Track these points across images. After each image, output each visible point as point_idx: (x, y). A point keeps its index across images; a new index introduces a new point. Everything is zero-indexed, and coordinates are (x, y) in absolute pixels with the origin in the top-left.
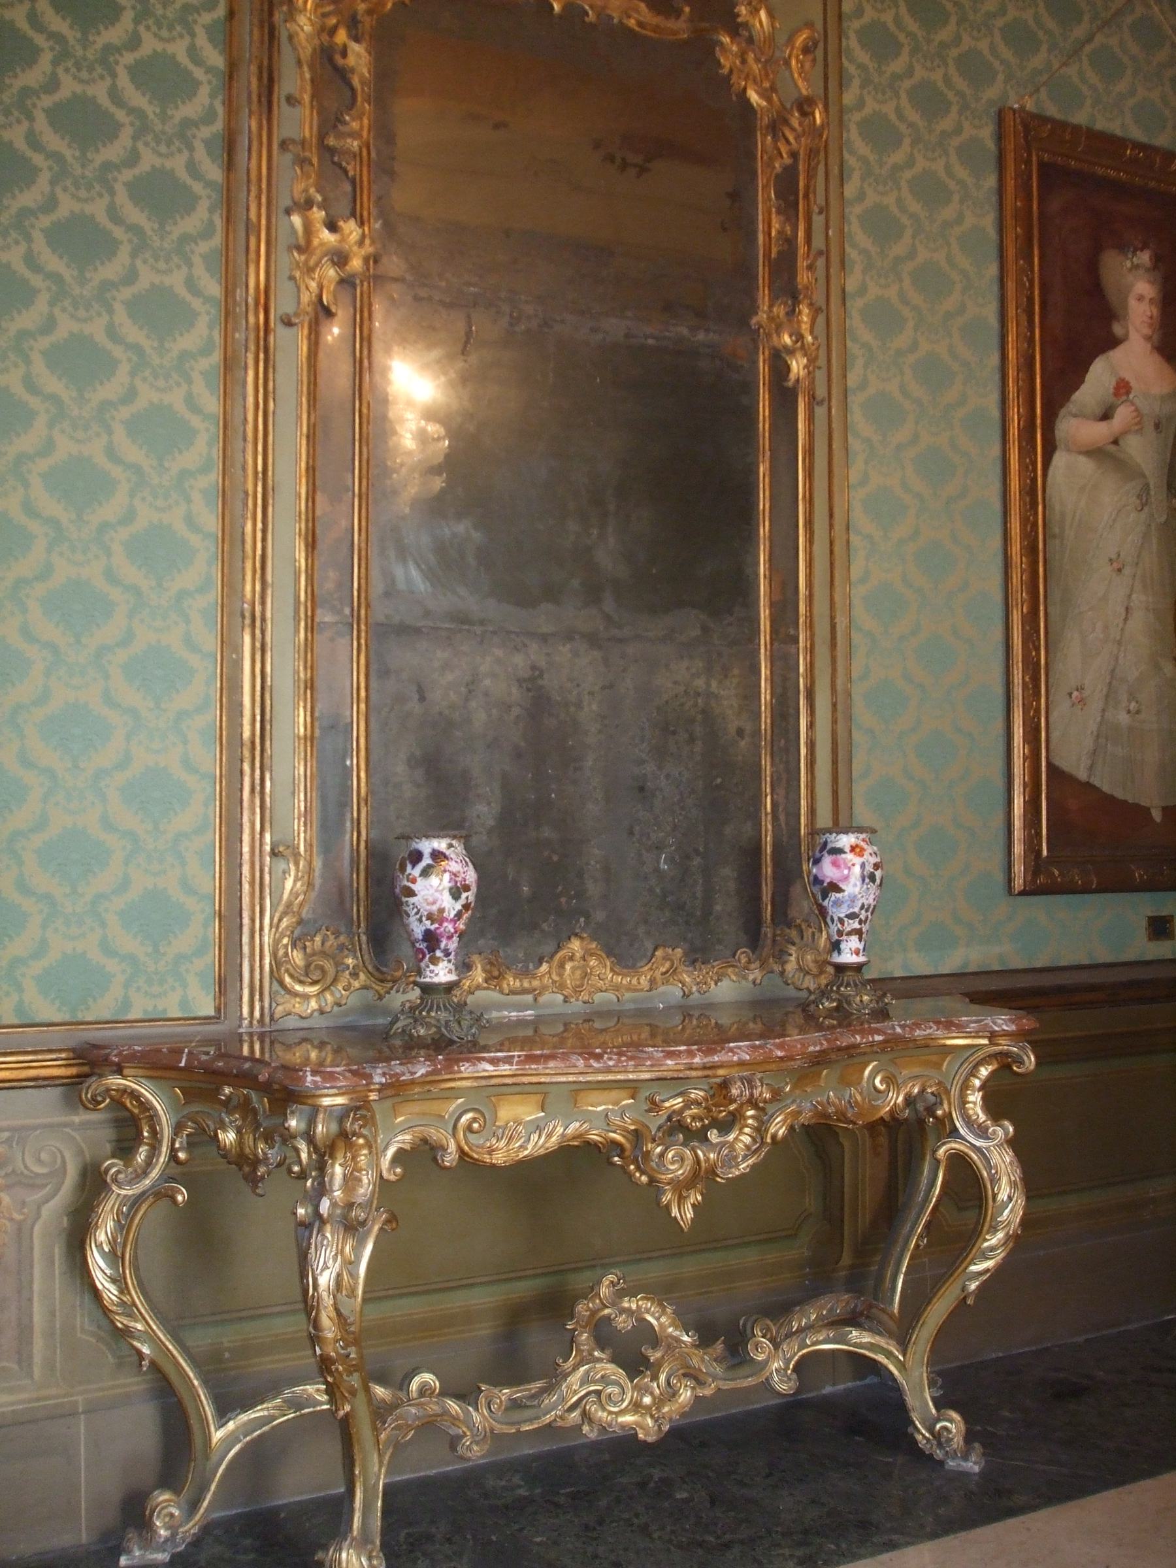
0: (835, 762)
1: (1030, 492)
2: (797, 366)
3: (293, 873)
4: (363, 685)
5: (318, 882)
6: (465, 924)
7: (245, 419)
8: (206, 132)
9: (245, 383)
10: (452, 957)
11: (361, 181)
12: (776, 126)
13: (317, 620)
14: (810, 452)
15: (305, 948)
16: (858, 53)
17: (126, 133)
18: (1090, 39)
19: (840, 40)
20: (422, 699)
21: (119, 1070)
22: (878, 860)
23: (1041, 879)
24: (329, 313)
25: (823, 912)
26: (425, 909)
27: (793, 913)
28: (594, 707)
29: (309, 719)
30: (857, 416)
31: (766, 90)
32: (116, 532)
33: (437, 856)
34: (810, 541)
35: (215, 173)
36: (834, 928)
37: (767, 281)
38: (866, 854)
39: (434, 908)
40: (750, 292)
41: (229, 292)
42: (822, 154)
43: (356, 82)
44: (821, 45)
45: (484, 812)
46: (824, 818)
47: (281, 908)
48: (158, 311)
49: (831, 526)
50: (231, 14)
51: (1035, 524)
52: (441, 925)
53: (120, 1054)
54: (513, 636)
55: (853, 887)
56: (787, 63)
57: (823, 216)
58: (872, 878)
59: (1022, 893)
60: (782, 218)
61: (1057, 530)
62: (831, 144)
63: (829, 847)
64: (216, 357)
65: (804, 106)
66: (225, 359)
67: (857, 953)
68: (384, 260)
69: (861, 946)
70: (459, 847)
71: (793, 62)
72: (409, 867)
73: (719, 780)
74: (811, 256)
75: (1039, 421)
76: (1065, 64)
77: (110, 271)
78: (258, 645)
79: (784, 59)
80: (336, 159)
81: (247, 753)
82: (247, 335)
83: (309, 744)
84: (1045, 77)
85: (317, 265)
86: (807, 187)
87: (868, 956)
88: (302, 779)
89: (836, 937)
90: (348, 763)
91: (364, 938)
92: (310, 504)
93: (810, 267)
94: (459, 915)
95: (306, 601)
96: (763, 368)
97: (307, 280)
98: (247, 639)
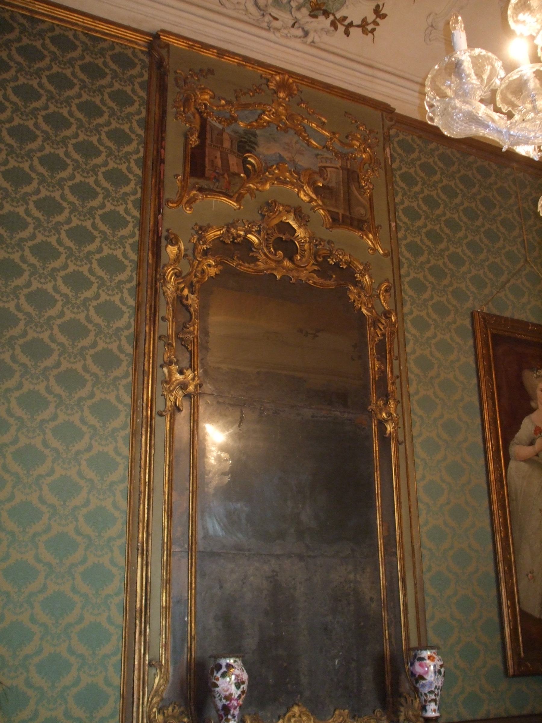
0: (417, 613)
1: (500, 480)
2: (390, 428)
3: (159, 675)
4: (193, 581)
5: (171, 679)
6: (243, 701)
7: (141, 458)
8: (126, 333)
9: (141, 441)
10: (236, 718)
11: (194, 351)
12: (375, 323)
13: (172, 550)
14: (398, 466)
15: (164, 713)
16: (408, 291)
17: (89, 384)
18: (508, 281)
19: (401, 285)
20: (221, 587)
22: (442, 663)
23: (522, 669)
24: (179, 410)
25: (416, 690)
26: (223, 694)
27: (402, 690)
28: (302, 589)
29: (168, 599)
30: (418, 449)
31: (370, 308)
32: (89, 351)
33: (229, 666)
34: (400, 507)
35: (130, 350)
36: (423, 698)
37: (374, 390)
38: (436, 660)
39: (227, 693)
40: (367, 395)
41: (134, 402)
42: (396, 334)
43: (192, 310)
44: (393, 288)
45: (250, 643)
46: (414, 643)
47: (152, 693)
48: (104, 411)
49: (409, 500)
50: (139, 284)
51: (504, 495)
52: (231, 701)
54: (263, 556)
55: (431, 677)
56: (378, 296)
57: (398, 361)
58: (439, 672)
59: (514, 676)
60: (379, 362)
61: (514, 498)
62: (399, 331)
63: (417, 657)
64: (128, 431)
65: (387, 314)
66: (132, 431)
67: (435, 711)
68: (204, 386)
69: (436, 708)
70: (240, 662)
71: (381, 296)
72: (215, 673)
73: (362, 624)
74: (393, 379)
75: (501, 448)
76: (498, 292)
77: (83, 393)
78: (144, 562)
79: (377, 295)
80: (183, 343)
81: (138, 615)
82: (143, 420)
83: (168, 610)
84: (491, 297)
85: (174, 389)
86: (390, 349)
87: (440, 713)
88: (164, 628)
89: (424, 703)
90: (186, 619)
91: (193, 708)
92: (170, 497)
93: (393, 383)
94: (239, 697)
95: (167, 542)
96: (375, 429)
97: (170, 396)
98: (139, 560)
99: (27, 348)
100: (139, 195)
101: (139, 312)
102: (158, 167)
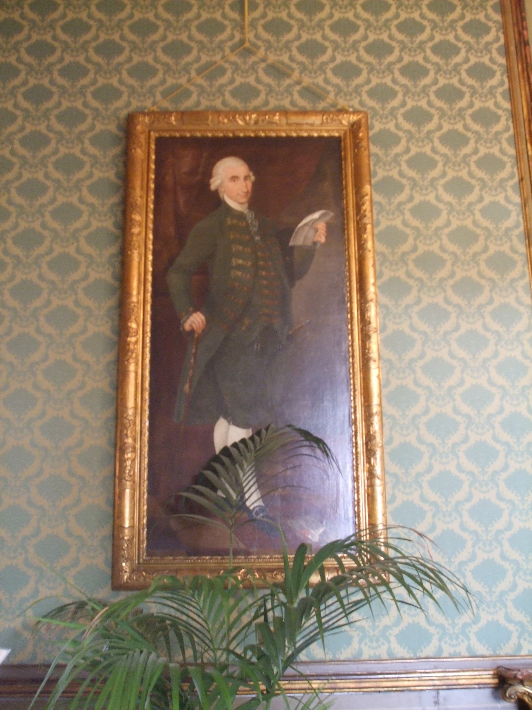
17: (487, 289)
21: (522, 682)
35: (507, 105)
50: (521, 180)
53: (522, 674)
64: (516, 179)
99: (420, 262)
100: (506, 86)
101: (527, 209)
102: (523, 51)
